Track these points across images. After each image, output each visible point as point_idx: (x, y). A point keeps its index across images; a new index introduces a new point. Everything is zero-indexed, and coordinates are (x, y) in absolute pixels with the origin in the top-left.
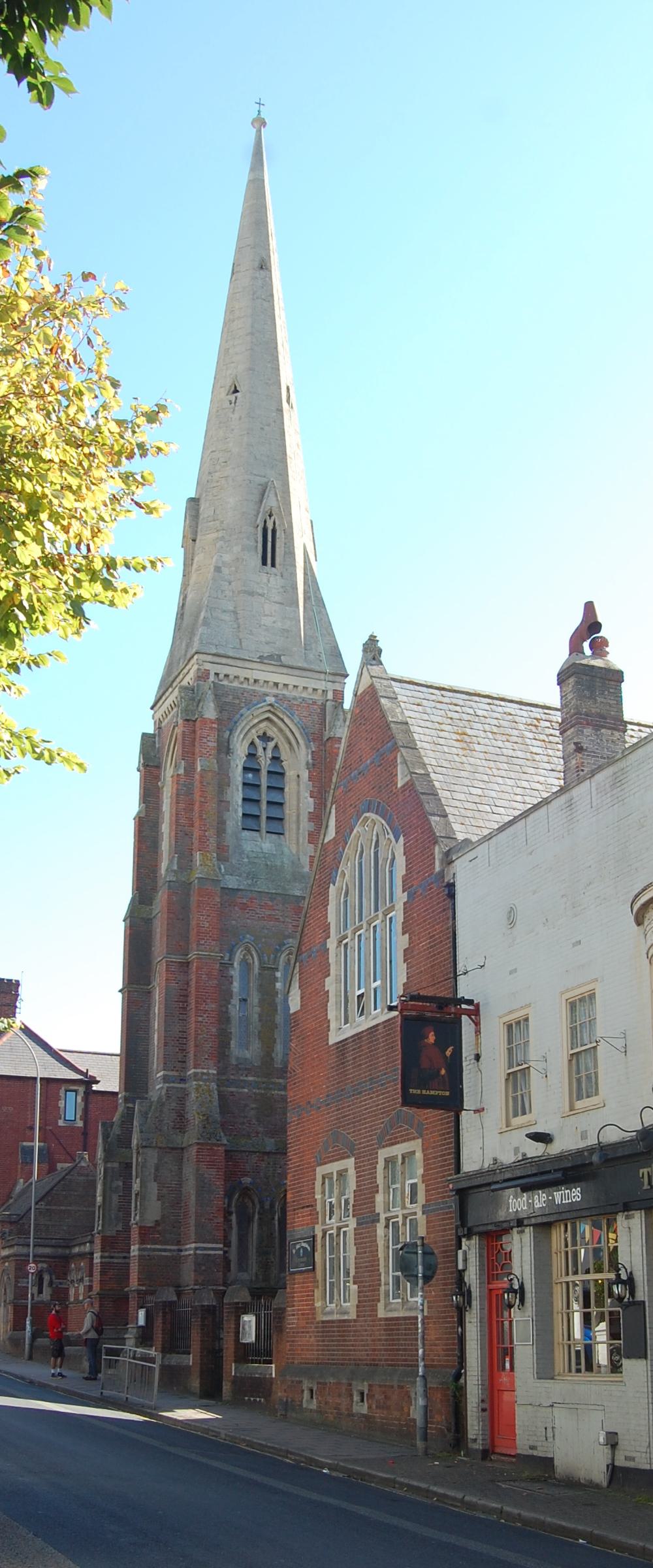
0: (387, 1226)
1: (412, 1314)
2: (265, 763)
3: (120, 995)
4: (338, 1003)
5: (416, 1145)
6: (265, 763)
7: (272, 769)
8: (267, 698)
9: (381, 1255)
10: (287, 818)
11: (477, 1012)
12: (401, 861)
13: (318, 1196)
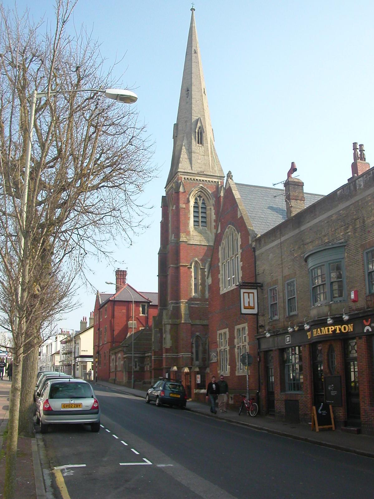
0: (238, 349)
1: (245, 374)
2: (200, 204)
3: (158, 277)
4: (223, 282)
5: (246, 325)
6: (200, 204)
7: (202, 206)
8: (200, 185)
9: (236, 357)
10: (207, 221)
11: (262, 286)
12: (239, 240)
13: (218, 340)
